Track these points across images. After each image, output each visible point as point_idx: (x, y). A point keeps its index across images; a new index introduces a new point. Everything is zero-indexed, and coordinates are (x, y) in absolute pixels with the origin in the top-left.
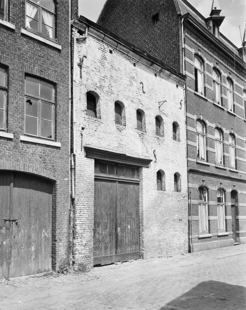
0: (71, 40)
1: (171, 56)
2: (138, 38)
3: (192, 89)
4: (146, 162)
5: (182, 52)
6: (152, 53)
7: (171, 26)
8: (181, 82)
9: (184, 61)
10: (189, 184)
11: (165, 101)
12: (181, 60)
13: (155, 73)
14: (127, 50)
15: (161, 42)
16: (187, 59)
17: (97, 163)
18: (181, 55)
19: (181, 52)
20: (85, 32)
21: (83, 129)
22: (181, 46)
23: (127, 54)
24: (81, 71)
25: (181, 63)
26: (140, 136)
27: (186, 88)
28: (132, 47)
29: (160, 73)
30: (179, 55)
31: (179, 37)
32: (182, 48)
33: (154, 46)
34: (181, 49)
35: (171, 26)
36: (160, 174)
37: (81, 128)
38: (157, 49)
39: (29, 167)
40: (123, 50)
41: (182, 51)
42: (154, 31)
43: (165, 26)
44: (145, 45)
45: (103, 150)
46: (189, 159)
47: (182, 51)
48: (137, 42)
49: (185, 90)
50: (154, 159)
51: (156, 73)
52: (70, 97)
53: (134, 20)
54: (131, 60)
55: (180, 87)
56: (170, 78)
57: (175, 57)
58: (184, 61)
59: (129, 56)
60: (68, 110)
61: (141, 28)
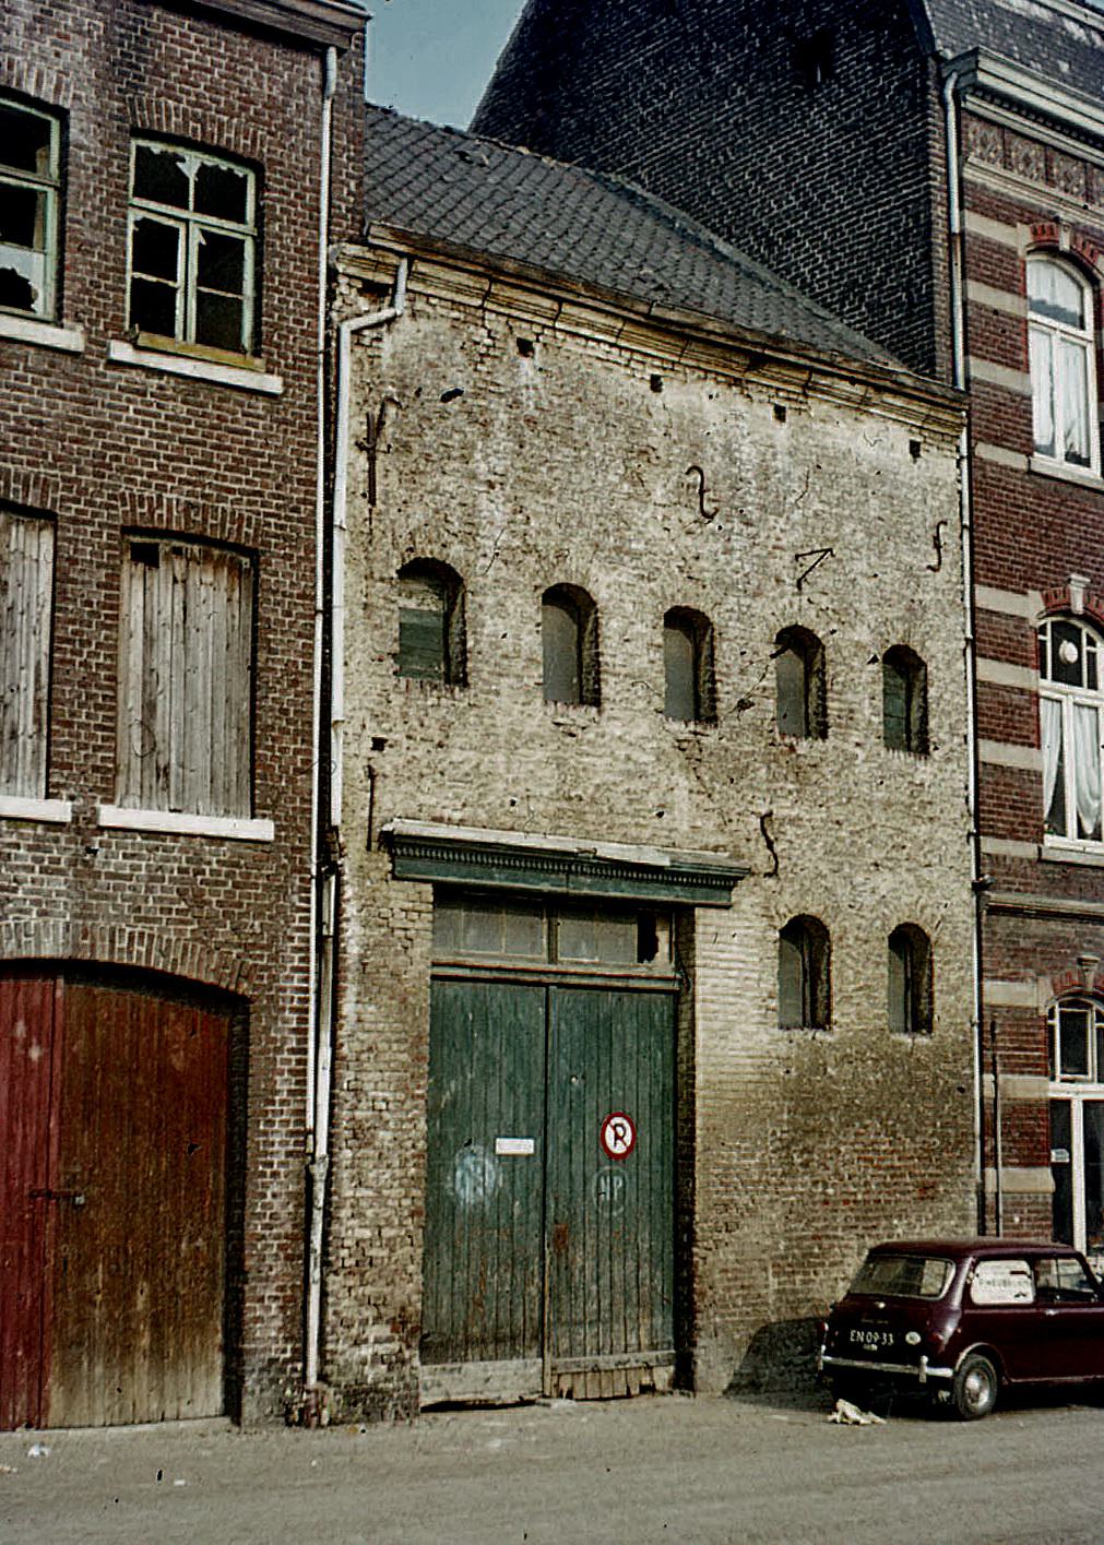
0: (328, 339)
1: (889, 274)
2: (725, 154)
3: (1010, 449)
4: (719, 883)
5: (950, 256)
6: (799, 247)
7: (893, 110)
8: (940, 425)
9: (958, 303)
10: (987, 985)
11: (826, 551)
12: (940, 303)
13: (776, 401)
14: (610, 321)
15: (841, 193)
16: (980, 293)
17: (446, 896)
18: (940, 268)
19: (941, 253)
20: (395, 286)
21: (379, 744)
22: (940, 226)
23: (612, 340)
24: (372, 472)
25: (941, 315)
26: (685, 745)
27: (970, 448)
28: (643, 308)
29: (807, 396)
30: (930, 272)
31: (929, 178)
32: (950, 236)
33: (804, 206)
34: (939, 238)
35: (893, 110)
36: (805, 938)
37: (371, 744)
38: (824, 229)
39: (131, 938)
40: (591, 325)
41: (950, 250)
42: (805, 126)
43: (859, 106)
44: (763, 201)
45: (477, 838)
46: (990, 845)
47: (950, 250)
48: (722, 180)
49: (965, 464)
50: (762, 860)
51: (784, 404)
52: (320, 605)
53: (706, 56)
54: (633, 364)
55: (934, 450)
56: (864, 417)
57: (910, 280)
58: (958, 303)
59: (621, 348)
60: (309, 665)
61: (741, 100)
